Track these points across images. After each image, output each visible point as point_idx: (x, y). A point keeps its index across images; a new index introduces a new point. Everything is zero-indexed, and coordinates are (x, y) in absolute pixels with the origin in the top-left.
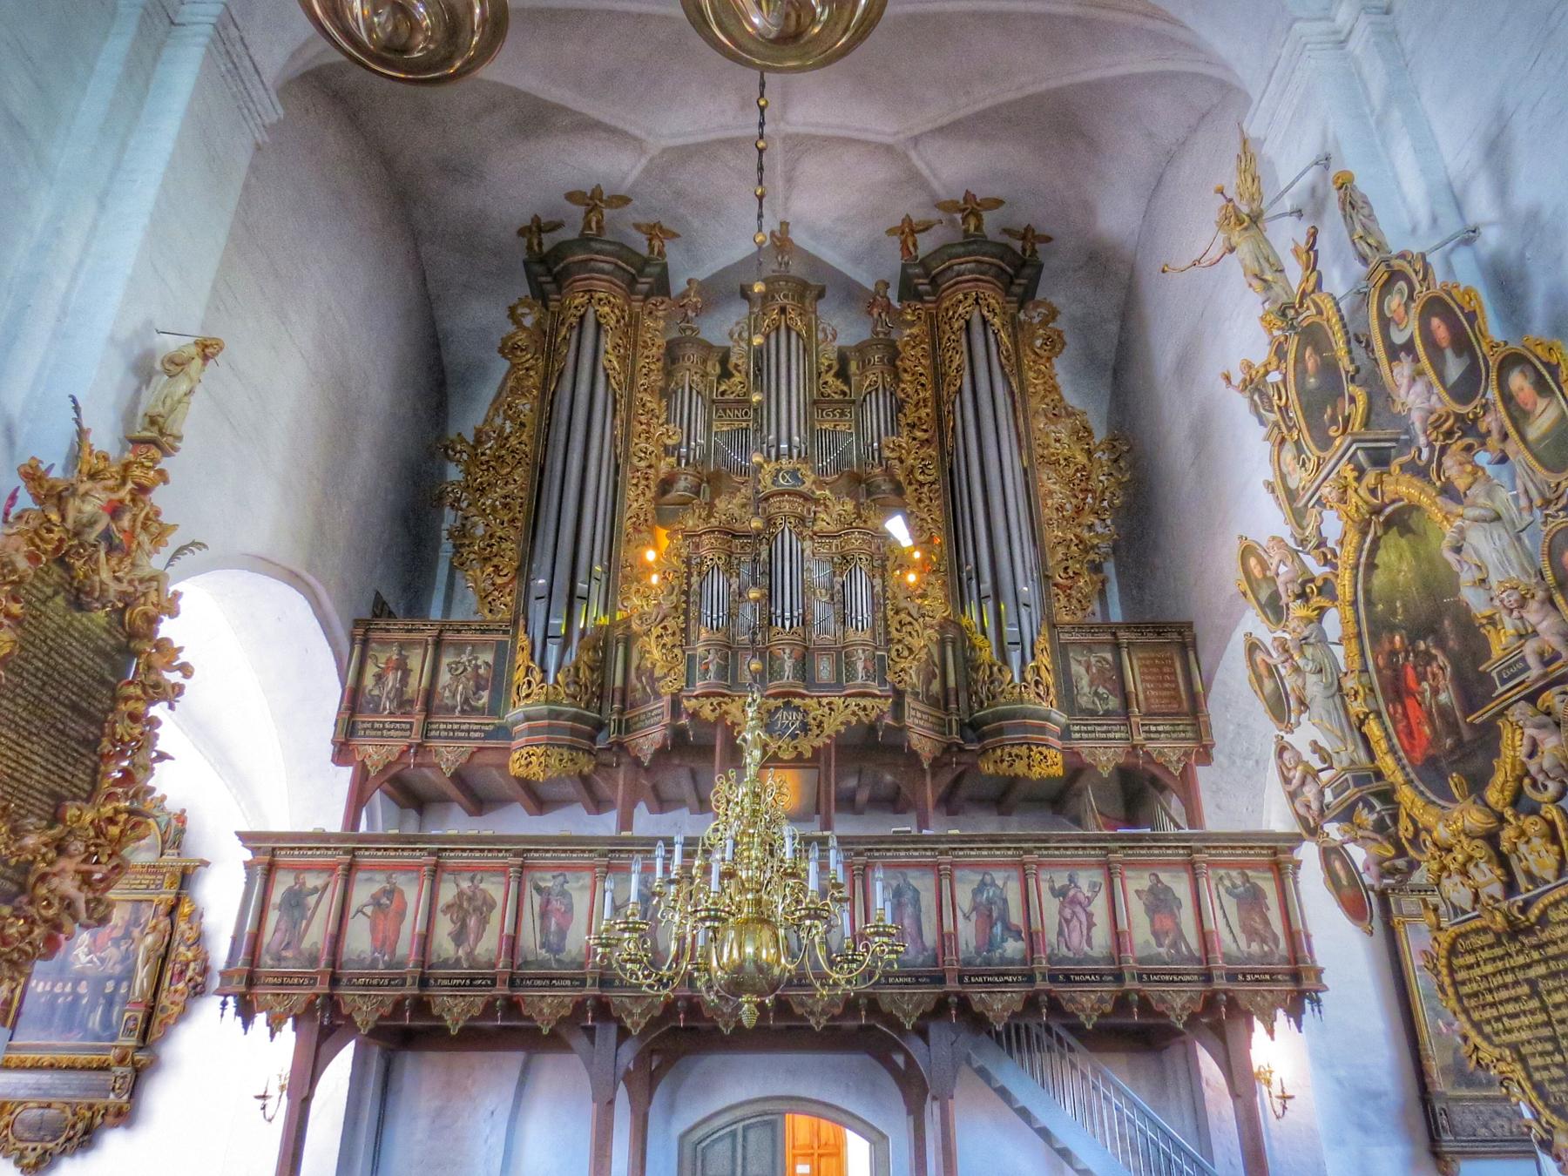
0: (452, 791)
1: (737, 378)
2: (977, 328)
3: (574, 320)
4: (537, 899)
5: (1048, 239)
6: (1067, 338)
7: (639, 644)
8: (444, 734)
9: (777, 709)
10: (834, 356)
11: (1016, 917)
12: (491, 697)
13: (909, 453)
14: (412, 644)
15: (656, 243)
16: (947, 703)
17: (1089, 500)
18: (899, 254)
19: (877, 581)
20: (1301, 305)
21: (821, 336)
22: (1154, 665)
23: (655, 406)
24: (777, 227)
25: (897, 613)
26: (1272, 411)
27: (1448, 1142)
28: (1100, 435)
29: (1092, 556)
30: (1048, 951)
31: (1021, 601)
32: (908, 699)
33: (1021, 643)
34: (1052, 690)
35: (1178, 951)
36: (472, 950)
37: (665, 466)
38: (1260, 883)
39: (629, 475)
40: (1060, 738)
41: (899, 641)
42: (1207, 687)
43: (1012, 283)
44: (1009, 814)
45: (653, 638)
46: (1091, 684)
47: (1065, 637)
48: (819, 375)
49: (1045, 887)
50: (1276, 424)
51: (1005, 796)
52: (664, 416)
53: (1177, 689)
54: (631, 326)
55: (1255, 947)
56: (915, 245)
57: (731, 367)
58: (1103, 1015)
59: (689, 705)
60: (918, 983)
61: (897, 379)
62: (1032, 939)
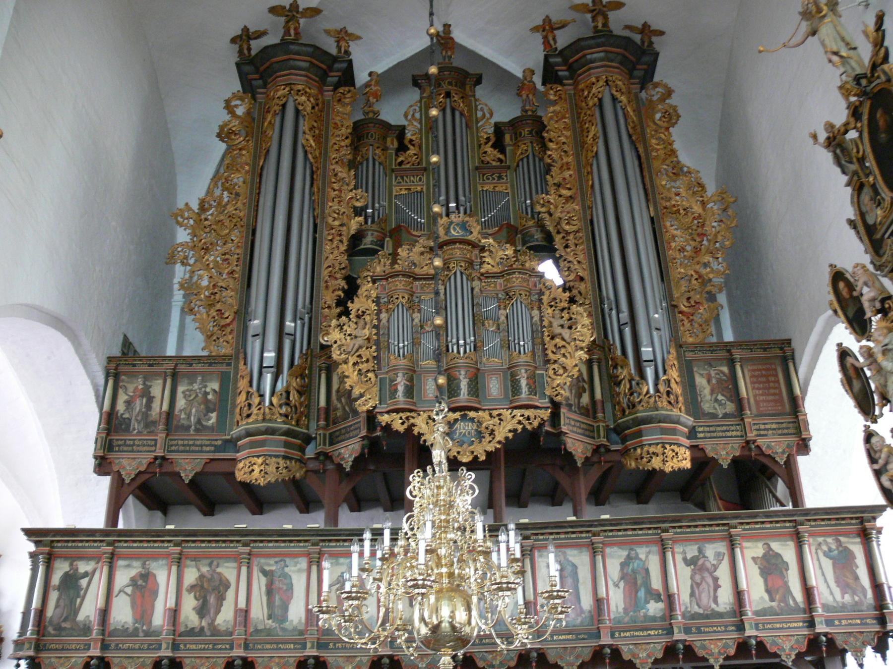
0: (191, 495)
1: (412, 151)
3: (277, 108)
5: (662, 33)
6: (680, 111)
7: (339, 370)
8: (182, 448)
9: (456, 420)
10: (491, 130)
11: (656, 583)
12: (218, 417)
13: (556, 207)
14: (156, 375)
15: (343, 44)
16: (595, 412)
17: (705, 242)
18: (542, 47)
19: (536, 312)
20: (873, 76)
21: (479, 114)
22: (762, 376)
23: (344, 175)
24: (441, 29)
25: (552, 338)
26: (851, 162)
28: (711, 189)
29: (708, 288)
30: (683, 609)
31: (653, 325)
32: (563, 410)
33: (654, 360)
34: (681, 399)
35: (787, 605)
36: (214, 620)
37: (355, 223)
38: (851, 547)
39: (325, 233)
40: (688, 438)
41: (555, 362)
42: (804, 392)
43: (634, 68)
44: (646, 503)
46: (712, 392)
47: (689, 355)
48: (480, 146)
49: (679, 558)
50: (855, 173)
51: (646, 486)
52: (353, 183)
53: (781, 393)
54: (322, 111)
55: (847, 598)
56: (554, 39)
57: (406, 142)
58: (727, 658)
59: (384, 419)
60: (577, 639)
61: (545, 148)
62: (670, 600)
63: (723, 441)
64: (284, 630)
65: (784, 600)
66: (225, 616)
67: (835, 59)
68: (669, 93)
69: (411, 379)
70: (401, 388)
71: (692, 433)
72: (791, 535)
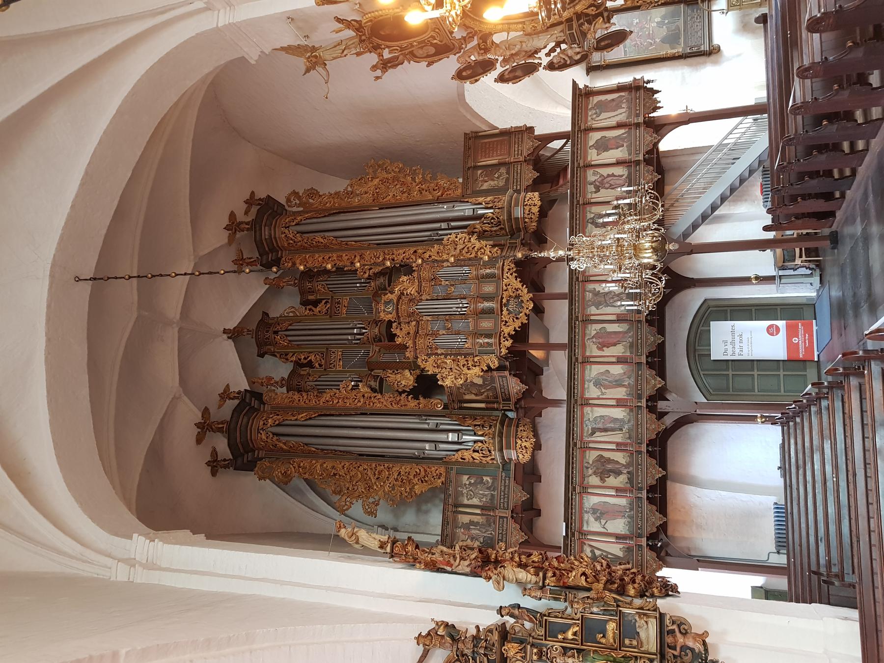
1: (312, 357)
2: (299, 228)
3: (275, 438)
4: (597, 434)
9: (507, 310)
21: (291, 314)
27: (705, 47)
35: (626, 138)
36: (623, 465)
38: (595, 102)
45: (468, 372)
46: (493, 180)
54: (278, 409)
59: (504, 351)
63: (523, 175)
64: (629, 421)
65: (623, 139)
66: (620, 458)
67: (345, 53)
68: (295, 193)
69: (482, 335)
70: (486, 340)
71: (518, 192)
72: (585, 134)
